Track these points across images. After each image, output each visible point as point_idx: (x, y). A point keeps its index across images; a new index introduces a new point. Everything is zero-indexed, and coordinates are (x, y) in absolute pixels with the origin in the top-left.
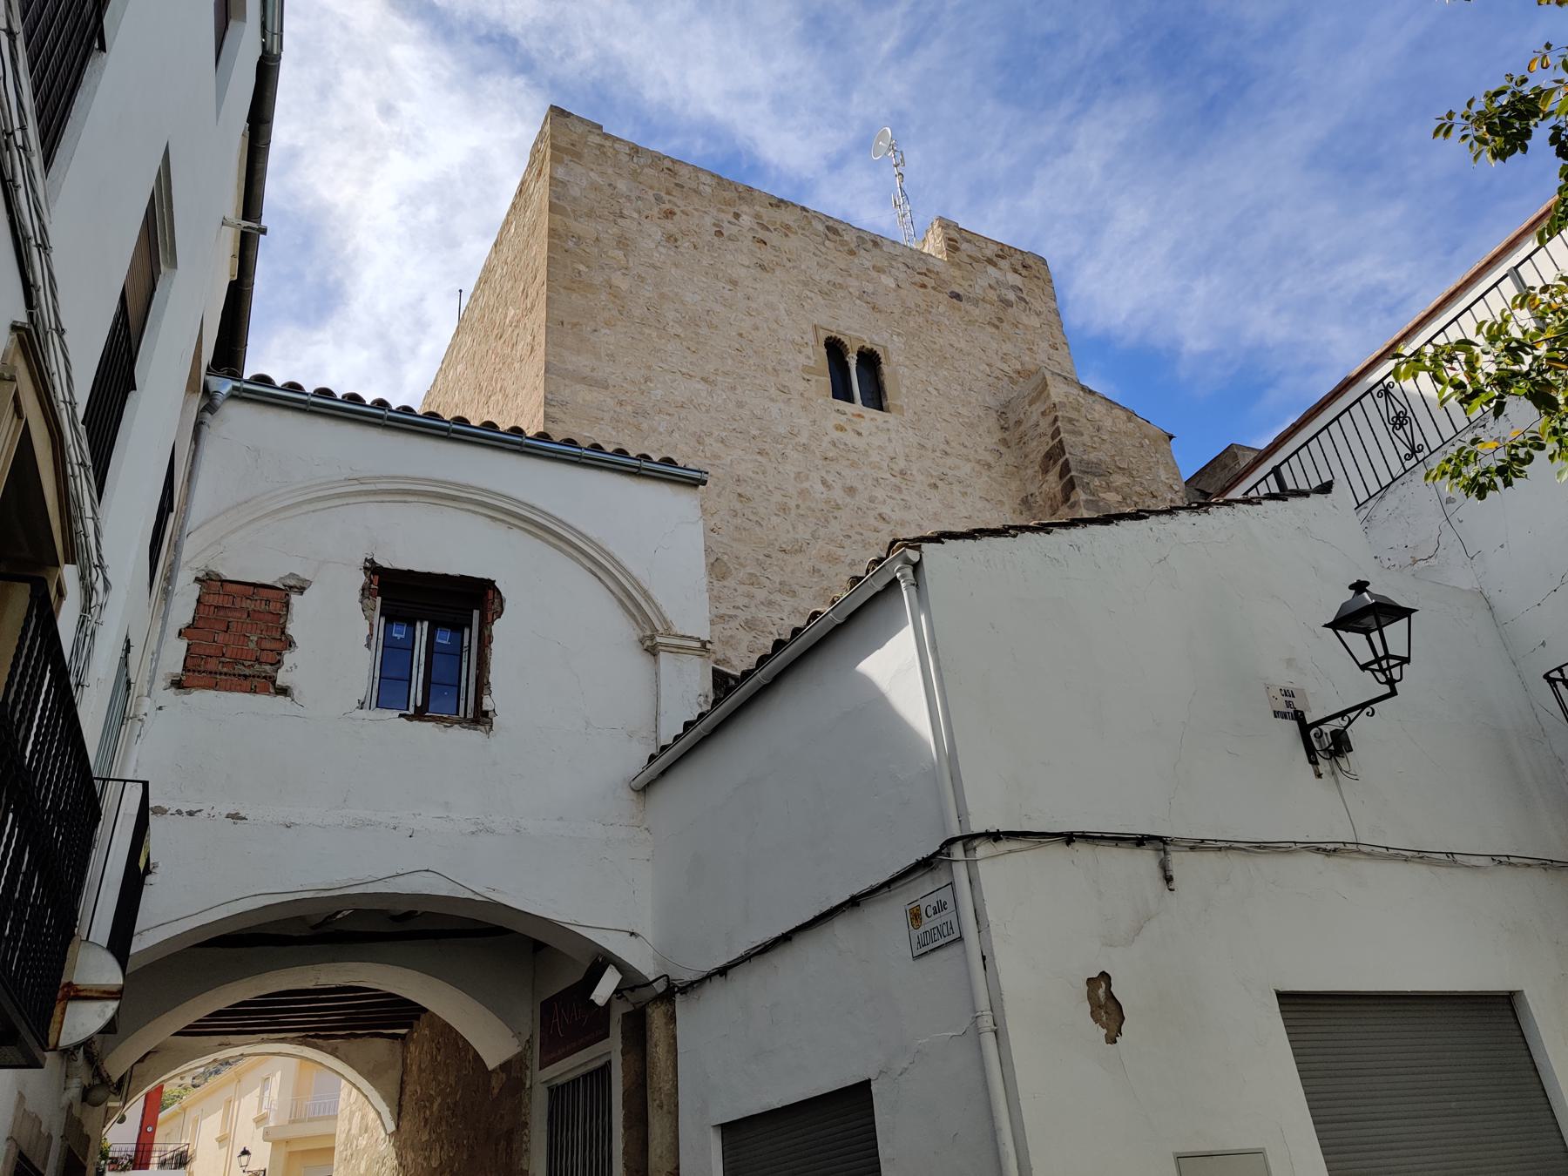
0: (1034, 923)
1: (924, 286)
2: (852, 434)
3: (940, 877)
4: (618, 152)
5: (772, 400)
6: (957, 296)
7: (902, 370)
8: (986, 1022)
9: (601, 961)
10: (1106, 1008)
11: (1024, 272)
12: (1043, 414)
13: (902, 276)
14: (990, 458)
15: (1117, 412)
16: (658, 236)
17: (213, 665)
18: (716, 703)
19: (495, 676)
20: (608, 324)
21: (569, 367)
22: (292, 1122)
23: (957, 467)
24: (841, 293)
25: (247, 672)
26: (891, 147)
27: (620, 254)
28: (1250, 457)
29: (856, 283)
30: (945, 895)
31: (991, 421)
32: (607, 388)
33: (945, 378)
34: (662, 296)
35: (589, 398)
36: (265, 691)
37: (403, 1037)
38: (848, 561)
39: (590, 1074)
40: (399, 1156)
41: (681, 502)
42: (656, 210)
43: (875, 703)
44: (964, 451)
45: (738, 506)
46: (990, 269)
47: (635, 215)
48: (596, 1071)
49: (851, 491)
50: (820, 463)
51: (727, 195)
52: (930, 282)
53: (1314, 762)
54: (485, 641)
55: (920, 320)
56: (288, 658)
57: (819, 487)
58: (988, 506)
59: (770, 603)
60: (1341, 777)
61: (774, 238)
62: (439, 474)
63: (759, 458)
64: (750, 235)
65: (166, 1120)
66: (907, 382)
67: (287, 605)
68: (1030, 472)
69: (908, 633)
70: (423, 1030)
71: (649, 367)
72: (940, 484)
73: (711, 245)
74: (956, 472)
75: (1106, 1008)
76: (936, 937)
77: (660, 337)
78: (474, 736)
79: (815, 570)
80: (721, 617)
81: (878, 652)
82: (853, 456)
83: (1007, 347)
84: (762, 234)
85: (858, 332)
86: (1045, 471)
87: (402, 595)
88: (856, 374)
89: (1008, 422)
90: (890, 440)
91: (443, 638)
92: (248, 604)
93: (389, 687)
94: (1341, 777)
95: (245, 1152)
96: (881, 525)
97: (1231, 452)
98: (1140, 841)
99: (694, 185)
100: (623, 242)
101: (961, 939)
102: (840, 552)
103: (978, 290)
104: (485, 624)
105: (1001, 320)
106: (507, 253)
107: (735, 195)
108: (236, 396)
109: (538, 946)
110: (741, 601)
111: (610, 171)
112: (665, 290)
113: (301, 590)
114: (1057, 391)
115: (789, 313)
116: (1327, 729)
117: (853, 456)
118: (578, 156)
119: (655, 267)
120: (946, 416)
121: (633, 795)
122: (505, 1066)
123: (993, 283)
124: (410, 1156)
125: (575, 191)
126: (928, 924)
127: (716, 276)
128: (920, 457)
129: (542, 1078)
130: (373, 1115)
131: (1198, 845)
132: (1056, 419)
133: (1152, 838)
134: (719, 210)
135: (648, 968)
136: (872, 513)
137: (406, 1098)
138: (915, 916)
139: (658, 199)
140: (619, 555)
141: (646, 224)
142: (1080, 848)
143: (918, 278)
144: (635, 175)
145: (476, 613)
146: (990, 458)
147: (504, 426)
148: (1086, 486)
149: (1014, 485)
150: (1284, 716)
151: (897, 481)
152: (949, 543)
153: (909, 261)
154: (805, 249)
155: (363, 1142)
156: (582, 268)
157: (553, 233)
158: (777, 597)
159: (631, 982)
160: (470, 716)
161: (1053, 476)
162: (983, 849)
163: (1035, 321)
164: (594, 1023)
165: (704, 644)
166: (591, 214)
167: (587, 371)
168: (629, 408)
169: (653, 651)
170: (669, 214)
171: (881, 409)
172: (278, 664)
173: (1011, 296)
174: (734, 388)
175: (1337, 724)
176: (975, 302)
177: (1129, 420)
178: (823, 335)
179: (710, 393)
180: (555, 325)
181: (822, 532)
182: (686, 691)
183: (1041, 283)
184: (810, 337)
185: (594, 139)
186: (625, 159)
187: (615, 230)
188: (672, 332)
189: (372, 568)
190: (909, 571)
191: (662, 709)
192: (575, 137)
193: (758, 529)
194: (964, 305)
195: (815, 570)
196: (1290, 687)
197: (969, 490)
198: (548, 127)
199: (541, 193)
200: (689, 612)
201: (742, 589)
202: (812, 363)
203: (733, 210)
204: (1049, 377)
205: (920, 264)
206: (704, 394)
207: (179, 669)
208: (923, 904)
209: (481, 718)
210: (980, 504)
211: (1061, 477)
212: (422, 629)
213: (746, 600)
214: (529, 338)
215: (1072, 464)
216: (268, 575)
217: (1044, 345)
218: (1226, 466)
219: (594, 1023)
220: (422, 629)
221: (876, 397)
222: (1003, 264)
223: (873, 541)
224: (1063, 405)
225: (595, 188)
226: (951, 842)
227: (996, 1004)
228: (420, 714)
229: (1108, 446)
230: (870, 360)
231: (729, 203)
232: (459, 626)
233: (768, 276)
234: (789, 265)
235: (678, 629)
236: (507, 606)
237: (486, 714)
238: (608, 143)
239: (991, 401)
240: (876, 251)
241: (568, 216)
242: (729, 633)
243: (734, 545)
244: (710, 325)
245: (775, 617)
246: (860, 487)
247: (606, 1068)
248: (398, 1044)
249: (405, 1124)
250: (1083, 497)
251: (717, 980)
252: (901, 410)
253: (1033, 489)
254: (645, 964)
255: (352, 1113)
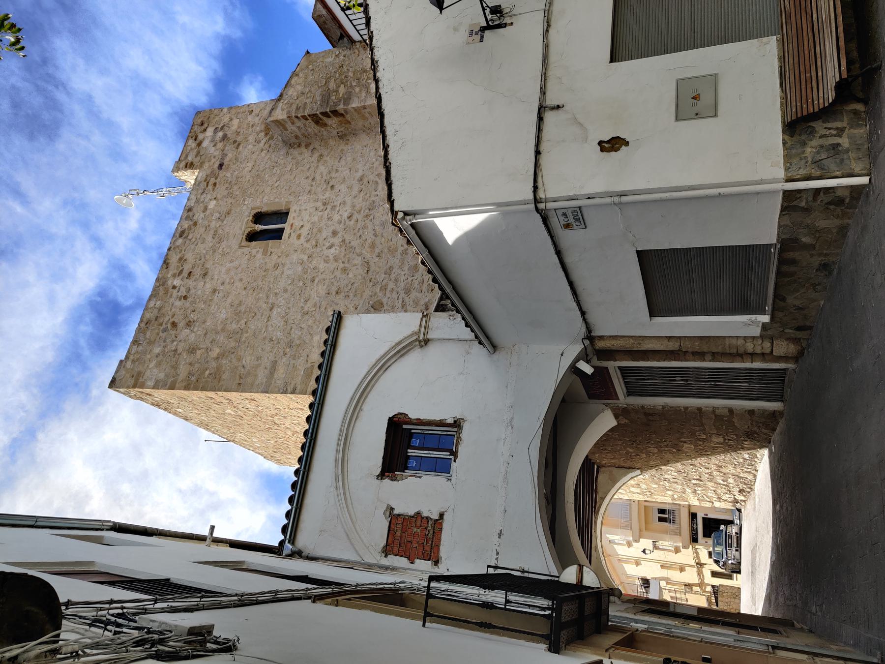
0: (577, 174)
1: (215, 184)
2: (302, 230)
3: (552, 214)
4: (137, 352)
5: (283, 273)
6: (221, 166)
7: (265, 200)
8: (616, 199)
9: (573, 369)
10: (613, 145)
11: (206, 125)
12: (293, 123)
13: (209, 196)
14: (316, 155)
15: (293, 81)
16: (187, 331)
17: (428, 548)
18: (458, 311)
19: (437, 417)
20: (239, 359)
21: (265, 380)
22: (631, 529)
23: (321, 174)
24: (220, 231)
25: (431, 532)
26: (127, 196)
27: (199, 353)
28: (319, 6)
29: (214, 223)
30: (560, 213)
31: (295, 152)
32: (276, 361)
33: (270, 176)
34: (223, 330)
35: (282, 371)
36: (441, 524)
37: (598, 467)
38: (373, 237)
39: (623, 376)
40: (651, 468)
41: (350, 324)
42: (171, 332)
43: (469, 238)
44: (312, 169)
45: (343, 294)
46: (205, 144)
47: (175, 343)
48: (622, 373)
49: (335, 233)
50: (318, 249)
51: (161, 292)
52: (212, 180)
53: (505, 25)
54: (419, 422)
55: (235, 188)
56: (425, 514)
57: (332, 250)
58: (344, 158)
59: (396, 280)
60: (512, 13)
61: (187, 267)
62: (334, 444)
63: (316, 282)
64: (186, 281)
65: (625, 590)
66: (272, 198)
67: (399, 515)
68: (325, 133)
69: (437, 221)
70: (596, 458)
71: (264, 338)
72: (331, 184)
73: (193, 302)
74: (325, 174)
75: (613, 145)
76: (577, 218)
77: (247, 332)
78: (466, 427)
79: (379, 256)
80: (403, 306)
81: (445, 235)
82: (315, 231)
83: (251, 139)
84: (185, 274)
85: (242, 224)
86: (325, 125)
87: (394, 463)
88: (267, 226)
89: (294, 143)
90: (306, 210)
91: (416, 442)
92: (398, 533)
93: (442, 468)
94: (512, 13)
95: (644, 551)
96: (354, 218)
97: (317, 18)
98: (540, 119)
99: (156, 311)
100: (192, 350)
101: (580, 207)
102: (369, 241)
103: (217, 153)
104: (410, 422)
105: (235, 142)
106: (193, 414)
107: (161, 288)
108: (292, 541)
109: (563, 400)
110: (395, 296)
111: (149, 356)
112: (219, 328)
113: (392, 509)
114: (280, 114)
115: (232, 261)
116: (489, 17)
117: (315, 231)
118: (139, 374)
119: (206, 334)
120: (292, 177)
121: (497, 352)
122: (616, 417)
123: (213, 144)
124: (652, 463)
125: (162, 375)
126: (571, 221)
127: (211, 300)
128: (322, 197)
129: (623, 399)
130: (632, 482)
131: (543, 90)
132: (297, 117)
133: (539, 113)
134: (171, 296)
135: (578, 348)
136: (348, 223)
137: (626, 465)
138: (568, 226)
139: (165, 330)
140: (378, 357)
141: (180, 337)
142: (542, 148)
143: (210, 187)
144: (151, 343)
145: (404, 426)
146: (316, 155)
147: (308, 412)
148: (336, 104)
149: (332, 142)
150: (482, 37)
151: (329, 207)
152: (394, 196)
153: (200, 192)
154: (194, 250)
155: (644, 486)
156: (207, 373)
157: (187, 388)
158: (393, 276)
159: (584, 356)
160: (456, 429)
161: (329, 121)
162: (541, 194)
163: (236, 122)
164: (601, 374)
165: (424, 316)
166: (175, 367)
167: (267, 372)
168: (288, 350)
169: (427, 341)
170: (174, 325)
171: (287, 213)
172: (428, 518)
173: (220, 134)
174: (276, 294)
175: (487, 11)
176: (224, 156)
177: (297, 75)
178: (245, 243)
179: (279, 306)
180: (240, 387)
181: (358, 250)
182: (449, 326)
183: (212, 116)
184: (246, 250)
185: (129, 364)
186: (140, 348)
187: (185, 355)
188: (243, 325)
189: (382, 476)
190: (408, 218)
191: (455, 337)
192: (128, 375)
193: (355, 285)
194: (226, 161)
195: (379, 256)
196: (467, 32)
197: (335, 168)
198: (121, 390)
199: (161, 394)
200: (408, 323)
201: (388, 295)
202: (261, 250)
203: (171, 290)
204: (272, 119)
205: (201, 185)
206: (279, 310)
207: (430, 562)
208: (562, 222)
209: (457, 424)
210: (343, 162)
211: (329, 116)
212: (411, 452)
213: (394, 293)
214: (247, 401)
215: (323, 110)
216: (383, 524)
217: (250, 118)
218: (325, 22)
219: (601, 374)
220: (411, 452)
221: (282, 216)
222: (201, 137)
223: (363, 223)
224: (288, 112)
225: (159, 364)
226: (537, 209)
227: (609, 195)
228: (455, 454)
229: (313, 89)
230: (259, 218)
231: (166, 292)
232: (410, 435)
233: (210, 274)
234: (203, 259)
235: (416, 329)
236: (402, 411)
237: (455, 422)
238: (131, 357)
239: (283, 152)
240: (194, 210)
241: (177, 380)
242: (411, 303)
243: (364, 298)
244: (240, 304)
245: (403, 278)
246: (332, 228)
247: (620, 368)
248: (601, 470)
249: (638, 465)
250: (341, 106)
251: (587, 316)
252: (289, 202)
253: (334, 132)
254: (577, 349)
255: (630, 492)
